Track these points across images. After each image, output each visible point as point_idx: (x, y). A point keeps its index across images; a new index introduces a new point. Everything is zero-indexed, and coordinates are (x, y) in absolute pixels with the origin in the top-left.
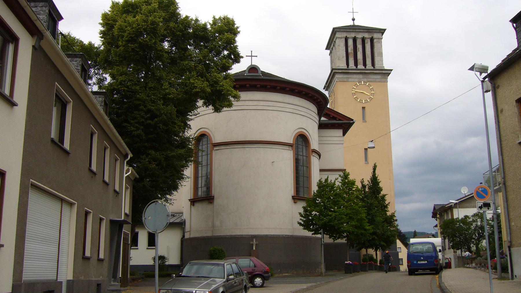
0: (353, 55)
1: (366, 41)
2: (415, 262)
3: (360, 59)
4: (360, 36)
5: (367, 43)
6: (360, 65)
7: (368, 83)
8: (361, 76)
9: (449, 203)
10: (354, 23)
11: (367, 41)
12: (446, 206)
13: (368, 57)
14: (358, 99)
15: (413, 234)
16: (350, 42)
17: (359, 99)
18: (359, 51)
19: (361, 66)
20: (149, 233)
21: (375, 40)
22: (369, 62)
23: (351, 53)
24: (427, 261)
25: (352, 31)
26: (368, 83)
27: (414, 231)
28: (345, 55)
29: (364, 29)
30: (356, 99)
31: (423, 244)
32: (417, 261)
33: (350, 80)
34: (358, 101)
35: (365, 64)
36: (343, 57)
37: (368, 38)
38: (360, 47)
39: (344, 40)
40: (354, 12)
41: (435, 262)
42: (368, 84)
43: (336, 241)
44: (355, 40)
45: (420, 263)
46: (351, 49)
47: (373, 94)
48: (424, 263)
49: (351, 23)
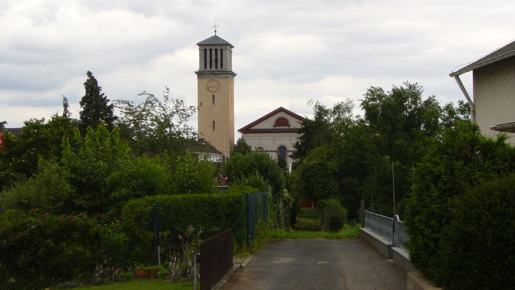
8: (212, 75)
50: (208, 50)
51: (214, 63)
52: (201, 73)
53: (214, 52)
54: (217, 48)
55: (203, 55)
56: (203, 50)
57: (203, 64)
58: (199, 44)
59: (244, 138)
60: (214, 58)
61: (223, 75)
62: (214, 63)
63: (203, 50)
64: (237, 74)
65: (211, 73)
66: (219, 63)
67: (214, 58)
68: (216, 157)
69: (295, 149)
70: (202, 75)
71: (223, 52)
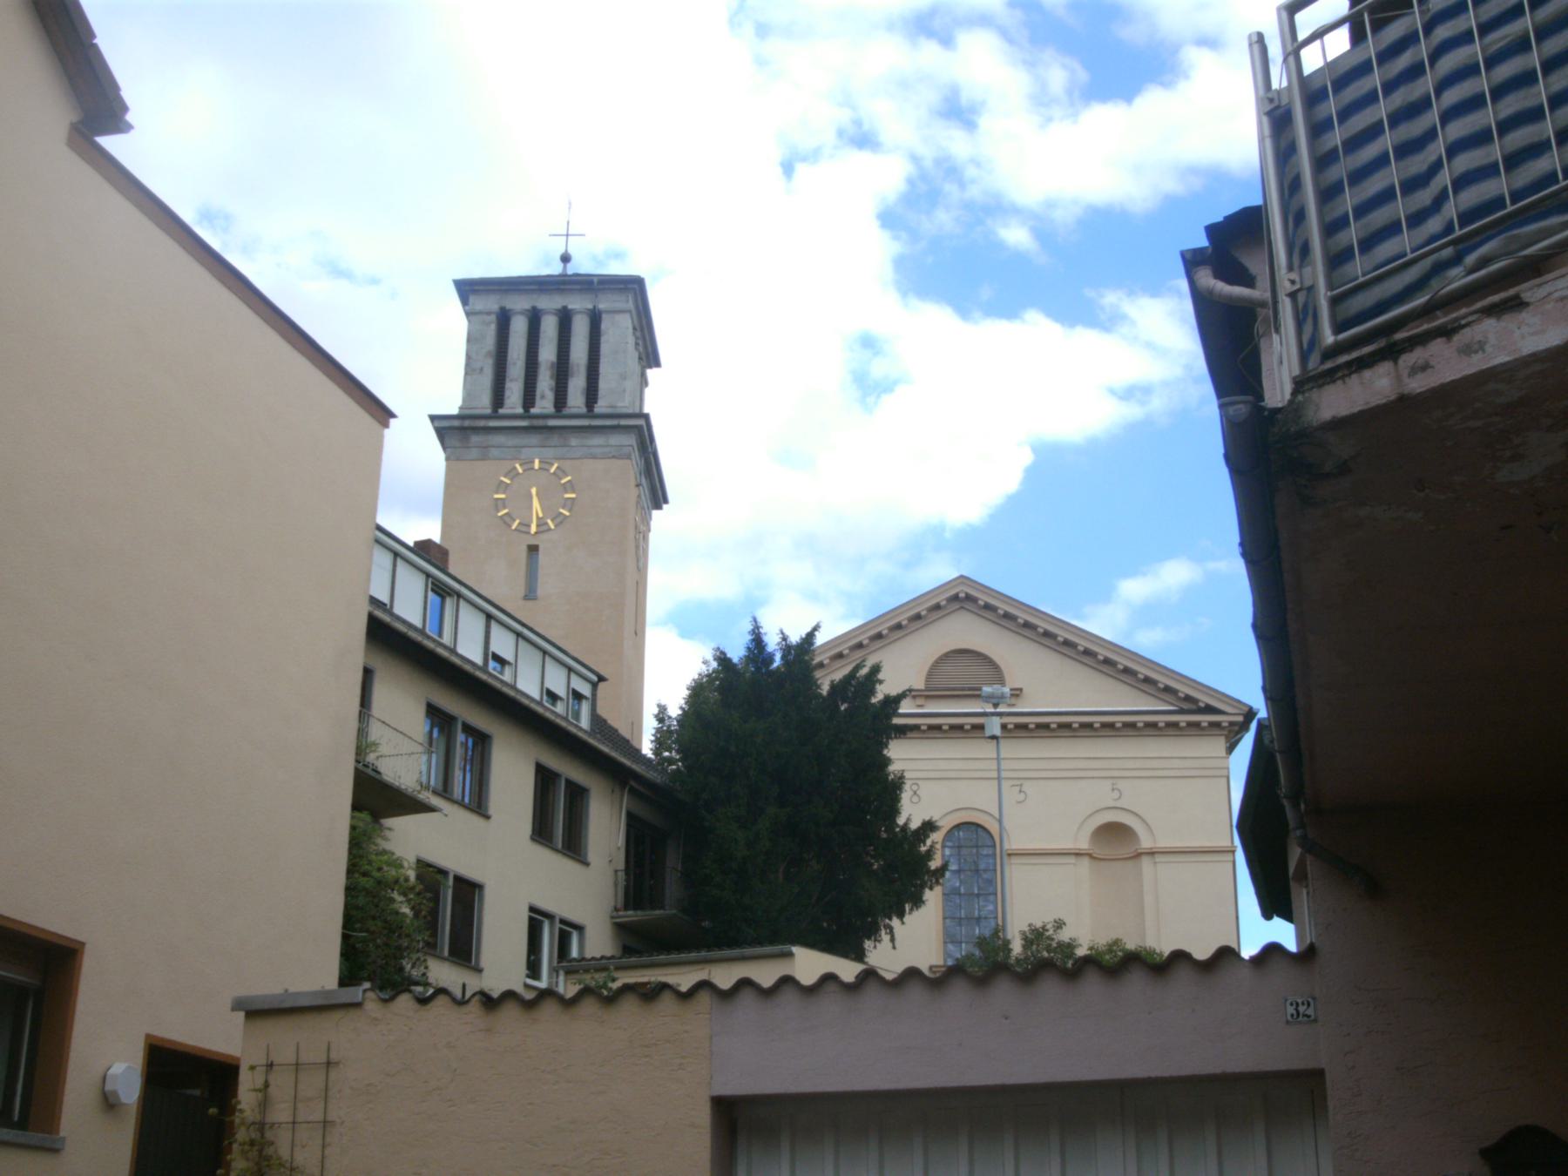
4: (519, 303)
7: (556, 465)
8: (534, 439)
10: (565, 268)
14: (514, 520)
17: (517, 522)
19: (545, 404)
20: (469, 959)
26: (556, 465)
29: (531, 283)
30: (506, 521)
31: (1158, 858)
33: (494, 452)
34: (514, 527)
37: (580, 312)
40: (570, 233)
42: (558, 468)
43: (1278, 755)
47: (569, 502)
49: (555, 269)
50: (521, 313)
51: (545, 384)
52: (467, 423)
53: (549, 327)
54: (570, 307)
55: (490, 341)
56: (489, 313)
57: (487, 379)
58: (468, 289)
59: (1223, 753)
60: (547, 353)
61: (597, 440)
62: (545, 384)
63: (489, 313)
64: (525, 915)
65: (522, 287)
66: (577, 385)
67: (547, 353)
68: (538, 655)
69: (1017, 947)
70: (475, 439)
71: (603, 326)
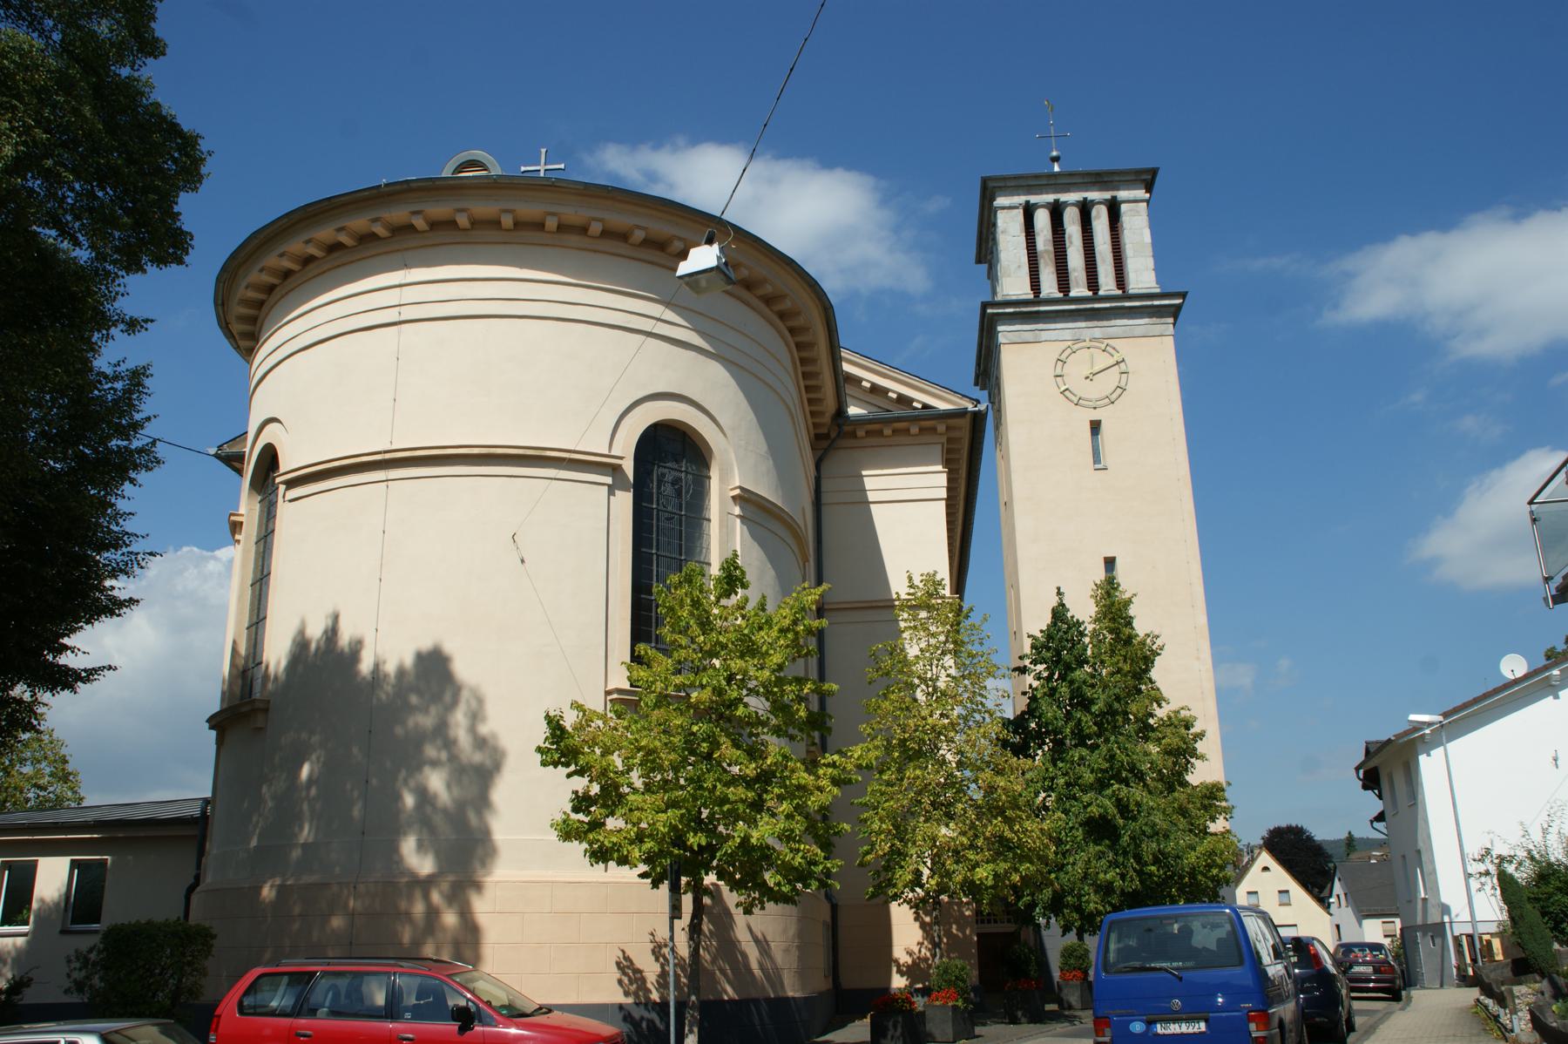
0: (1054, 259)
1: (1094, 213)
2: (1137, 1027)
3: (1075, 270)
5: (1098, 217)
6: (1078, 287)
9: (1408, 727)
11: (1098, 212)
12: (1401, 741)
13: (1104, 261)
15: (1344, 848)
16: (1042, 219)
18: (1071, 243)
19: (1079, 289)
21: (1124, 207)
22: (1106, 277)
23: (1046, 251)
24: (1206, 1021)
25: (1045, 182)
27: (1347, 835)
28: (1025, 259)
32: (1150, 1023)
33: (1044, 336)
35: (1093, 282)
36: (1019, 267)
38: (1073, 229)
39: (1020, 212)
41: (1252, 1026)
44: (1056, 211)
45: (1168, 1032)
46: (1045, 241)
48: (1191, 1030)
